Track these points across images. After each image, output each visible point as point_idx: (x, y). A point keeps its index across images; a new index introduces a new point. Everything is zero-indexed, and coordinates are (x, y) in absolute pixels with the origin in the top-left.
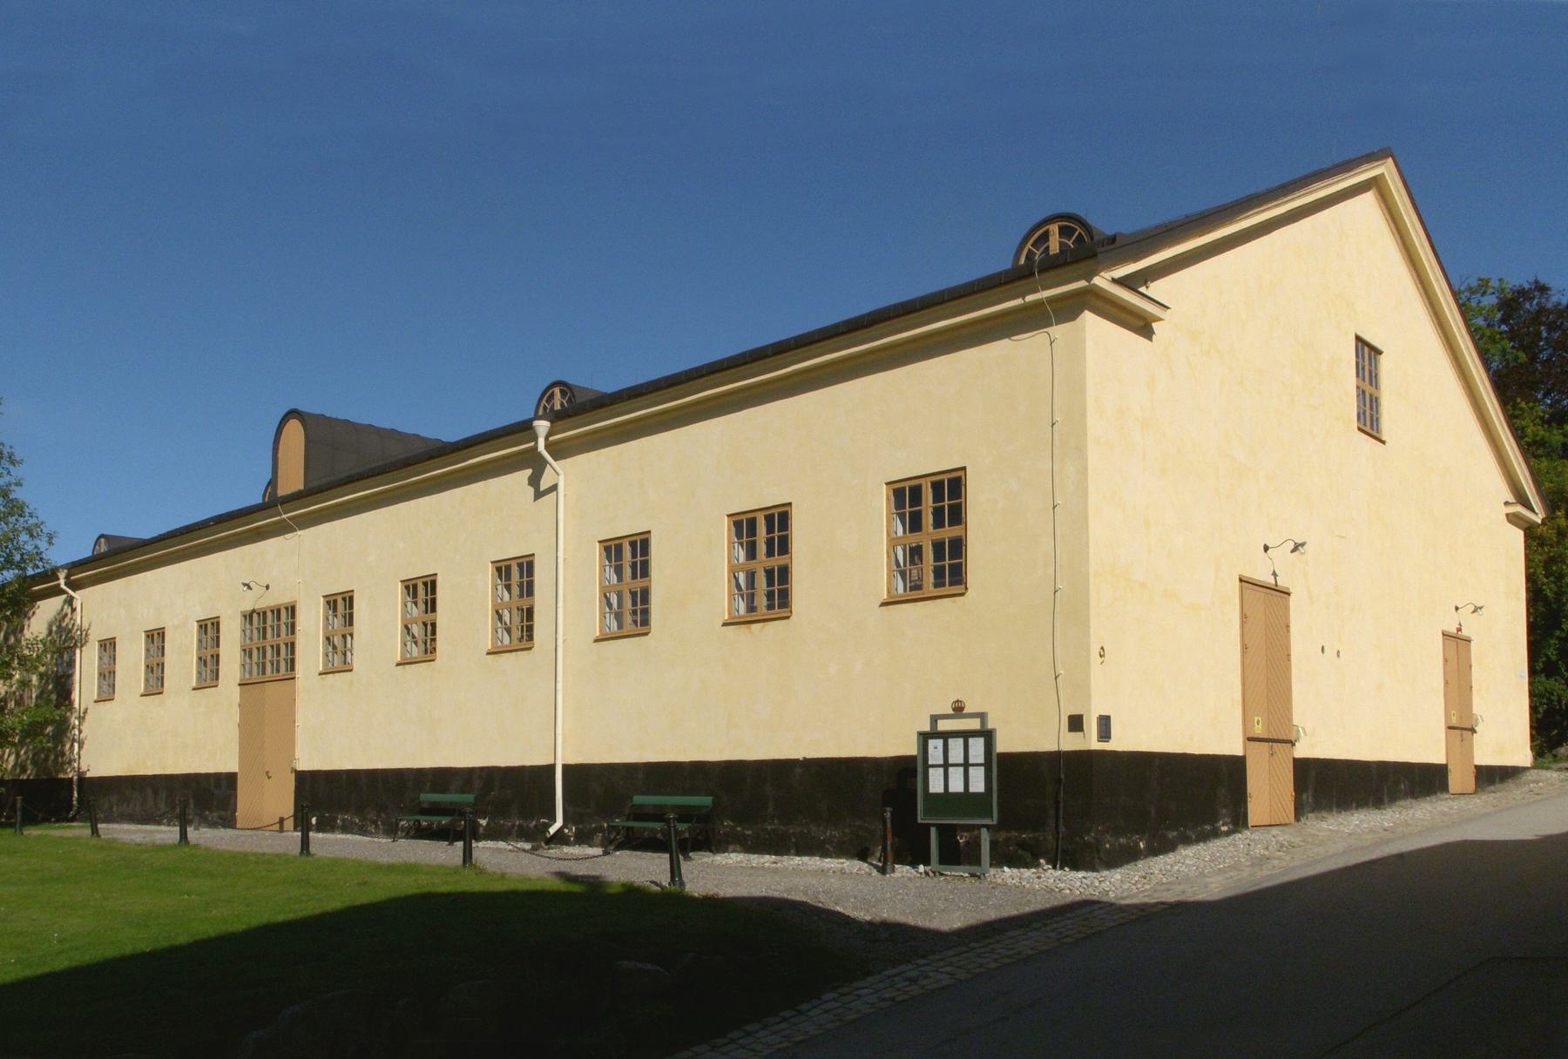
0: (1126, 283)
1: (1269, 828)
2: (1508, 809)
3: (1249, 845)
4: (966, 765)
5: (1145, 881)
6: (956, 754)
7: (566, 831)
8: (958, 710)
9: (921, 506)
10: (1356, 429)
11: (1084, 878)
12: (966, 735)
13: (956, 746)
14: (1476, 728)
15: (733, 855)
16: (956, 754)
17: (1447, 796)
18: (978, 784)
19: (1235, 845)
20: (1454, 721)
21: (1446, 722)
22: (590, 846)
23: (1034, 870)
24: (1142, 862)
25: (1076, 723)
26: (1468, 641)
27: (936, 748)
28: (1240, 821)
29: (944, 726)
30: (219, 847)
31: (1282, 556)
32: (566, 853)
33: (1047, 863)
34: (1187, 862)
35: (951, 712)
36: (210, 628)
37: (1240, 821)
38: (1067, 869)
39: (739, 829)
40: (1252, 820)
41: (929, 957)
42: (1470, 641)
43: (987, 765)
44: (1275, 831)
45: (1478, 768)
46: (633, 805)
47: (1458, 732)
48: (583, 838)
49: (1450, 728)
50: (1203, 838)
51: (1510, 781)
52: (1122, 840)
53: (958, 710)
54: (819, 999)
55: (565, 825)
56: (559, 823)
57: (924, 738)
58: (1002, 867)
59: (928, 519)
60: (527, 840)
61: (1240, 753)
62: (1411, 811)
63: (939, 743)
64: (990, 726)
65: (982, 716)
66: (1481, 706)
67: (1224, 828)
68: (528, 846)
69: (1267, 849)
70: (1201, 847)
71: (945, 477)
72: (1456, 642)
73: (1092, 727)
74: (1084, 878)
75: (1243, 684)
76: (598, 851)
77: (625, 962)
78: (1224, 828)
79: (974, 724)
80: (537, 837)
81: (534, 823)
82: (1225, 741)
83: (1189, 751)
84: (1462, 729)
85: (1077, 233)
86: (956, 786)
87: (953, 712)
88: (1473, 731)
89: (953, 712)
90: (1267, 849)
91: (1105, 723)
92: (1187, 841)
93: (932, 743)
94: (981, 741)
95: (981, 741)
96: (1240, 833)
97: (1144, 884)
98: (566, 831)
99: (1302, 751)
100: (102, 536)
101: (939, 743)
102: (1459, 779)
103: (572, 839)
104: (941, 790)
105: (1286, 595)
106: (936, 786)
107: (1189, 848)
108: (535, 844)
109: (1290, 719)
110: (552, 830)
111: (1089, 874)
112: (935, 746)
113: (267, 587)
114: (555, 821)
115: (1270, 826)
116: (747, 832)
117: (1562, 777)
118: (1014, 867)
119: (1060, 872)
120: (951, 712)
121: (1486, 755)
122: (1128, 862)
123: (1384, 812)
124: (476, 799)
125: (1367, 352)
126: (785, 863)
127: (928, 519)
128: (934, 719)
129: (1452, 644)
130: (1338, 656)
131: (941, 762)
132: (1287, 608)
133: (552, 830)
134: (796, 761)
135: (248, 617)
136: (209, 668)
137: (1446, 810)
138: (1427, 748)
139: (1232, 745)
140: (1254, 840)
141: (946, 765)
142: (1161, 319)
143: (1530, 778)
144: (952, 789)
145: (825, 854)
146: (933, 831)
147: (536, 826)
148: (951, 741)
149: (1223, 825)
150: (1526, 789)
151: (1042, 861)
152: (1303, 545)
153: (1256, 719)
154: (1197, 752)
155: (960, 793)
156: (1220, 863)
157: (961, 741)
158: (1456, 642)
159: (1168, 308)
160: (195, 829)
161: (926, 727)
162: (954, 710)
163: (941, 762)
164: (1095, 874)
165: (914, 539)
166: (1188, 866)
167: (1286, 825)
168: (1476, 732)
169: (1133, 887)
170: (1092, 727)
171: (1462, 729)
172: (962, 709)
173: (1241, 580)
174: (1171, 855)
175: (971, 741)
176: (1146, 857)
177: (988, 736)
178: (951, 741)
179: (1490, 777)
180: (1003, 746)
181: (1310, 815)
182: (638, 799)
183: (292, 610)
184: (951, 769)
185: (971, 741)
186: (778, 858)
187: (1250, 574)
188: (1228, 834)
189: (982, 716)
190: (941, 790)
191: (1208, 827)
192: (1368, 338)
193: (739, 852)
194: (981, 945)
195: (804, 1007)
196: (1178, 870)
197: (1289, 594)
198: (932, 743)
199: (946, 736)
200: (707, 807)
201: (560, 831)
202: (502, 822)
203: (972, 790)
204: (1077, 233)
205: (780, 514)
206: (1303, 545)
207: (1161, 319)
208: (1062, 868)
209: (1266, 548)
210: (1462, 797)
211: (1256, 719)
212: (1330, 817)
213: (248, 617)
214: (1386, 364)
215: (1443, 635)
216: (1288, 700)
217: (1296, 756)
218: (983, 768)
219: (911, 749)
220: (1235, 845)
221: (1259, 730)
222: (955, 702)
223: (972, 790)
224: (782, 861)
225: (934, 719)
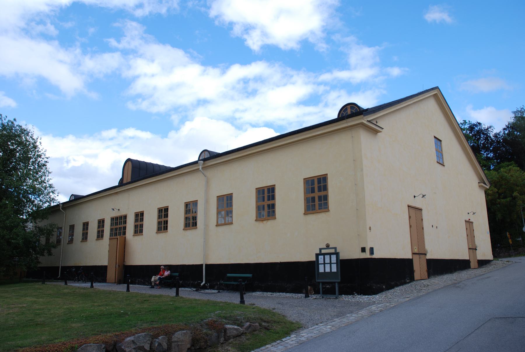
0: (371, 122)
1: (421, 281)
2: (489, 273)
3: (415, 286)
4: (331, 263)
5: (386, 298)
6: (327, 260)
7: (206, 285)
8: (328, 246)
9: (314, 185)
10: (436, 162)
11: (368, 297)
12: (330, 254)
13: (327, 257)
14: (477, 248)
15: (258, 292)
16: (327, 260)
17: (470, 269)
18: (334, 269)
19: (411, 286)
20: (471, 247)
21: (468, 247)
22: (213, 290)
23: (352, 295)
24: (384, 292)
25: (363, 250)
26: (472, 223)
27: (321, 258)
28: (412, 279)
29: (323, 251)
30: (153, 294)
31: (419, 198)
32: (206, 292)
33: (356, 293)
34: (398, 292)
35: (325, 247)
36: (101, 223)
37: (412, 279)
38: (362, 295)
39: (260, 284)
40: (415, 279)
41: (319, 325)
42: (473, 223)
43: (337, 263)
44: (422, 281)
45: (478, 260)
46: (227, 277)
47: (472, 250)
48: (212, 287)
49: (469, 249)
50: (402, 284)
51: (488, 264)
52: (379, 285)
53: (328, 246)
54: (290, 336)
55: (206, 283)
56: (204, 283)
57: (317, 255)
58: (342, 295)
59: (316, 189)
60: (194, 288)
61: (411, 258)
62: (461, 274)
63: (322, 257)
64: (338, 251)
65: (335, 248)
66: (477, 242)
67: (408, 281)
68: (194, 289)
69: (421, 287)
70: (401, 287)
71: (322, 177)
72: (469, 223)
73: (368, 250)
74: (368, 297)
75: (411, 237)
76: (216, 291)
77: (228, 326)
78: (408, 281)
79: (333, 251)
80: (198, 288)
81: (196, 282)
82: (407, 255)
83: (396, 258)
84: (473, 249)
85: (355, 108)
86: (328, 270)
87: (326, 247)
88: (476, 249)
89: (326, 247)
90: (421, 287)
91: (372, 250)
92: (397, 286)
93: (320, 257)
94: (335, 256)
95: (335, 256)
96: (412, 282)
97: (386, 299)
98: (206, 285)
99: (429, 257)
100: (72, 195)
101: (322, 257)
102: (473, 264)
103: (208, 287)
104: (323, 271)
105: (421, 210)
106: (321, 270)
107: (398, 287)
108: (197, 289)
109: (424, 247)
110: (202, 284)
111: (369, 296)
112: (321, 258)
113: (119, 210)
114: (203, 282)
115: (421, 280)
116: (263, 285)
117: (503, 263)
118: (346, 295)
119: (360, 296)
120: (325, 247)
121: (480, 257)
122: (380, 292)
123: (453, 275)
124: (179, 275)
125: (438, 140)
126: (81, 285)
127: (316, 189)
128: (321, 250)
129: (468, 224)
130: (437, 227)
131: (323, 263)
132: (421, 214)
133: (202, 284)
134: (277, 263)
135: (112, 219)
136: (100, 235)
137: (471, 273)
138: (463, 254)
139: (409, 256)
140: (417, 284)
141: (324, 264)
142: (382, 132)
143: (493, 263)
144: (326, 271)
145: (287, 292)
146: (337, 285)
147: (197, 283)
148: (326, 256)
149: (407, 280)
150: (493, 266)
151: (354, 293)
152: (425, 195)
153: (415, 247)
154: (398, 258)
155: (329, 272)
156: (407, 292)
157: (329, 256)
158: (469, 223)
159: (383, 129)
160: (43, 283)
161: (318, 252)
162: (326, 246)
163: (323, 263)
164: (371, 296)
165: (312, 195)
166: (398, 293)
167: (425, 279)
168: (477, 250)
169: (383, 300)
170: (368, 250)
171: (473, 249)
172: (329, 246)
173: (408, 206)
174: (393, 290)
175: (332, 256)
176: (385, 290)
177: (337, 254)
178: (326, 256)
179: (482, 263)
180: (343, 256)
181: (432, 276)
182: (229, 275)
183: (125, 217)
184: (326, 265)
185: (332, 256)
186: (272, 293)
187: (410, 204)
188: (409, 283)
189: (335, 248)
190: (323, 271)
191: (403, 281)
192: (441, 166)
193: (260, 292)
194: (338, 319)
195: (283, 340)
196: (395, 294)
197: (421, 210)
198: (320, 257)
199: (324, 254)
200: (250, 277)
201: (204, 285)
202: (186, 282)
203: (333, 271)
204: (355, 108)
205: (272, 188)
206: (425, 195)
207: (382, 132)
208: (360, 295)
209: (415, 197)
210: (475, 269)
211: (415, 247)
212: (438, 277)
213: (112, 219)
214: (443, 143)
215: (465, 221)
216: (424, 245)
217: (427, 258)
218: (336, 264)
219: (314, 259)
220: (411, 286)
221: (416, 251)
222: (327, 244)
223: (333, 271)
224: (273, 294)
225: (321, 250)
